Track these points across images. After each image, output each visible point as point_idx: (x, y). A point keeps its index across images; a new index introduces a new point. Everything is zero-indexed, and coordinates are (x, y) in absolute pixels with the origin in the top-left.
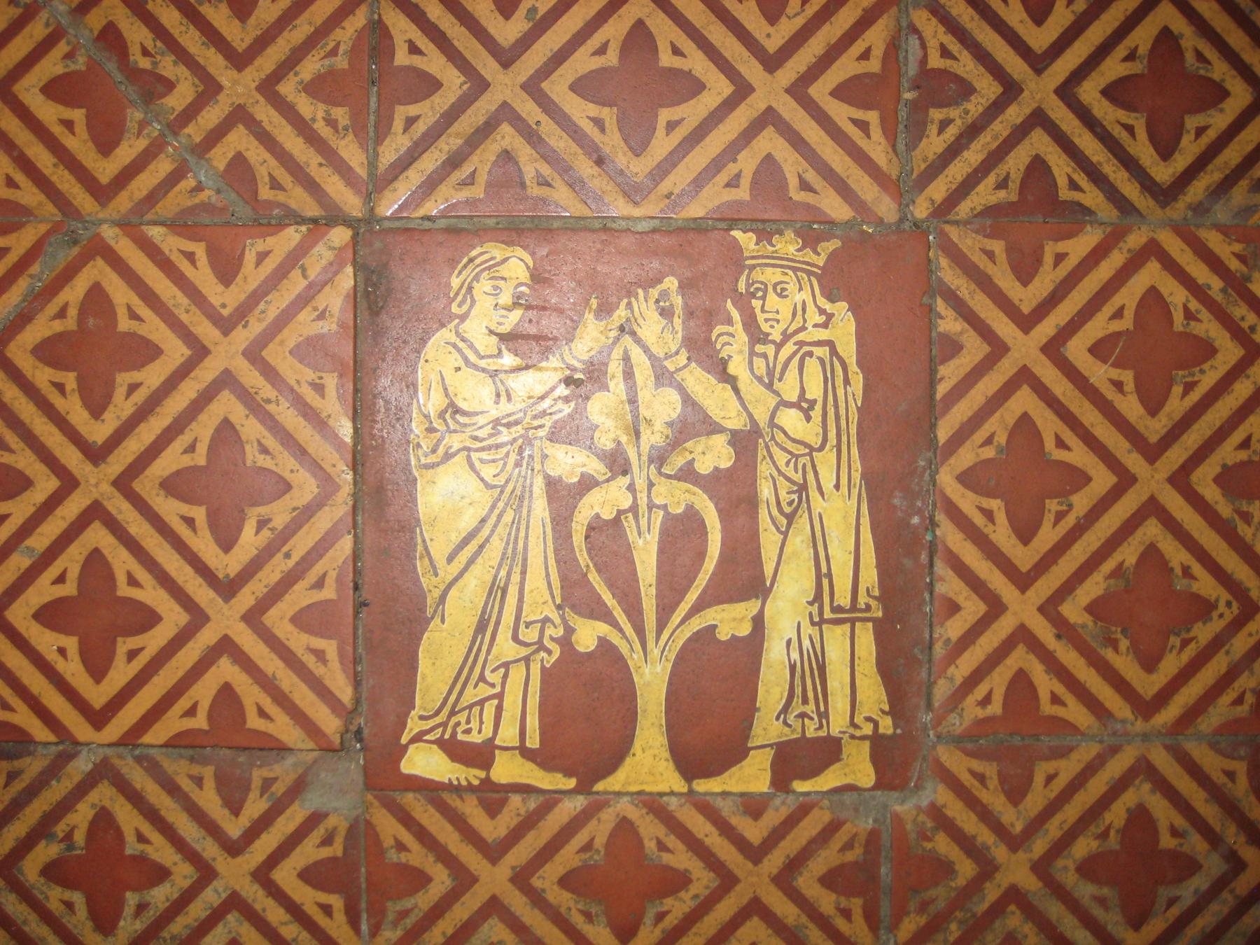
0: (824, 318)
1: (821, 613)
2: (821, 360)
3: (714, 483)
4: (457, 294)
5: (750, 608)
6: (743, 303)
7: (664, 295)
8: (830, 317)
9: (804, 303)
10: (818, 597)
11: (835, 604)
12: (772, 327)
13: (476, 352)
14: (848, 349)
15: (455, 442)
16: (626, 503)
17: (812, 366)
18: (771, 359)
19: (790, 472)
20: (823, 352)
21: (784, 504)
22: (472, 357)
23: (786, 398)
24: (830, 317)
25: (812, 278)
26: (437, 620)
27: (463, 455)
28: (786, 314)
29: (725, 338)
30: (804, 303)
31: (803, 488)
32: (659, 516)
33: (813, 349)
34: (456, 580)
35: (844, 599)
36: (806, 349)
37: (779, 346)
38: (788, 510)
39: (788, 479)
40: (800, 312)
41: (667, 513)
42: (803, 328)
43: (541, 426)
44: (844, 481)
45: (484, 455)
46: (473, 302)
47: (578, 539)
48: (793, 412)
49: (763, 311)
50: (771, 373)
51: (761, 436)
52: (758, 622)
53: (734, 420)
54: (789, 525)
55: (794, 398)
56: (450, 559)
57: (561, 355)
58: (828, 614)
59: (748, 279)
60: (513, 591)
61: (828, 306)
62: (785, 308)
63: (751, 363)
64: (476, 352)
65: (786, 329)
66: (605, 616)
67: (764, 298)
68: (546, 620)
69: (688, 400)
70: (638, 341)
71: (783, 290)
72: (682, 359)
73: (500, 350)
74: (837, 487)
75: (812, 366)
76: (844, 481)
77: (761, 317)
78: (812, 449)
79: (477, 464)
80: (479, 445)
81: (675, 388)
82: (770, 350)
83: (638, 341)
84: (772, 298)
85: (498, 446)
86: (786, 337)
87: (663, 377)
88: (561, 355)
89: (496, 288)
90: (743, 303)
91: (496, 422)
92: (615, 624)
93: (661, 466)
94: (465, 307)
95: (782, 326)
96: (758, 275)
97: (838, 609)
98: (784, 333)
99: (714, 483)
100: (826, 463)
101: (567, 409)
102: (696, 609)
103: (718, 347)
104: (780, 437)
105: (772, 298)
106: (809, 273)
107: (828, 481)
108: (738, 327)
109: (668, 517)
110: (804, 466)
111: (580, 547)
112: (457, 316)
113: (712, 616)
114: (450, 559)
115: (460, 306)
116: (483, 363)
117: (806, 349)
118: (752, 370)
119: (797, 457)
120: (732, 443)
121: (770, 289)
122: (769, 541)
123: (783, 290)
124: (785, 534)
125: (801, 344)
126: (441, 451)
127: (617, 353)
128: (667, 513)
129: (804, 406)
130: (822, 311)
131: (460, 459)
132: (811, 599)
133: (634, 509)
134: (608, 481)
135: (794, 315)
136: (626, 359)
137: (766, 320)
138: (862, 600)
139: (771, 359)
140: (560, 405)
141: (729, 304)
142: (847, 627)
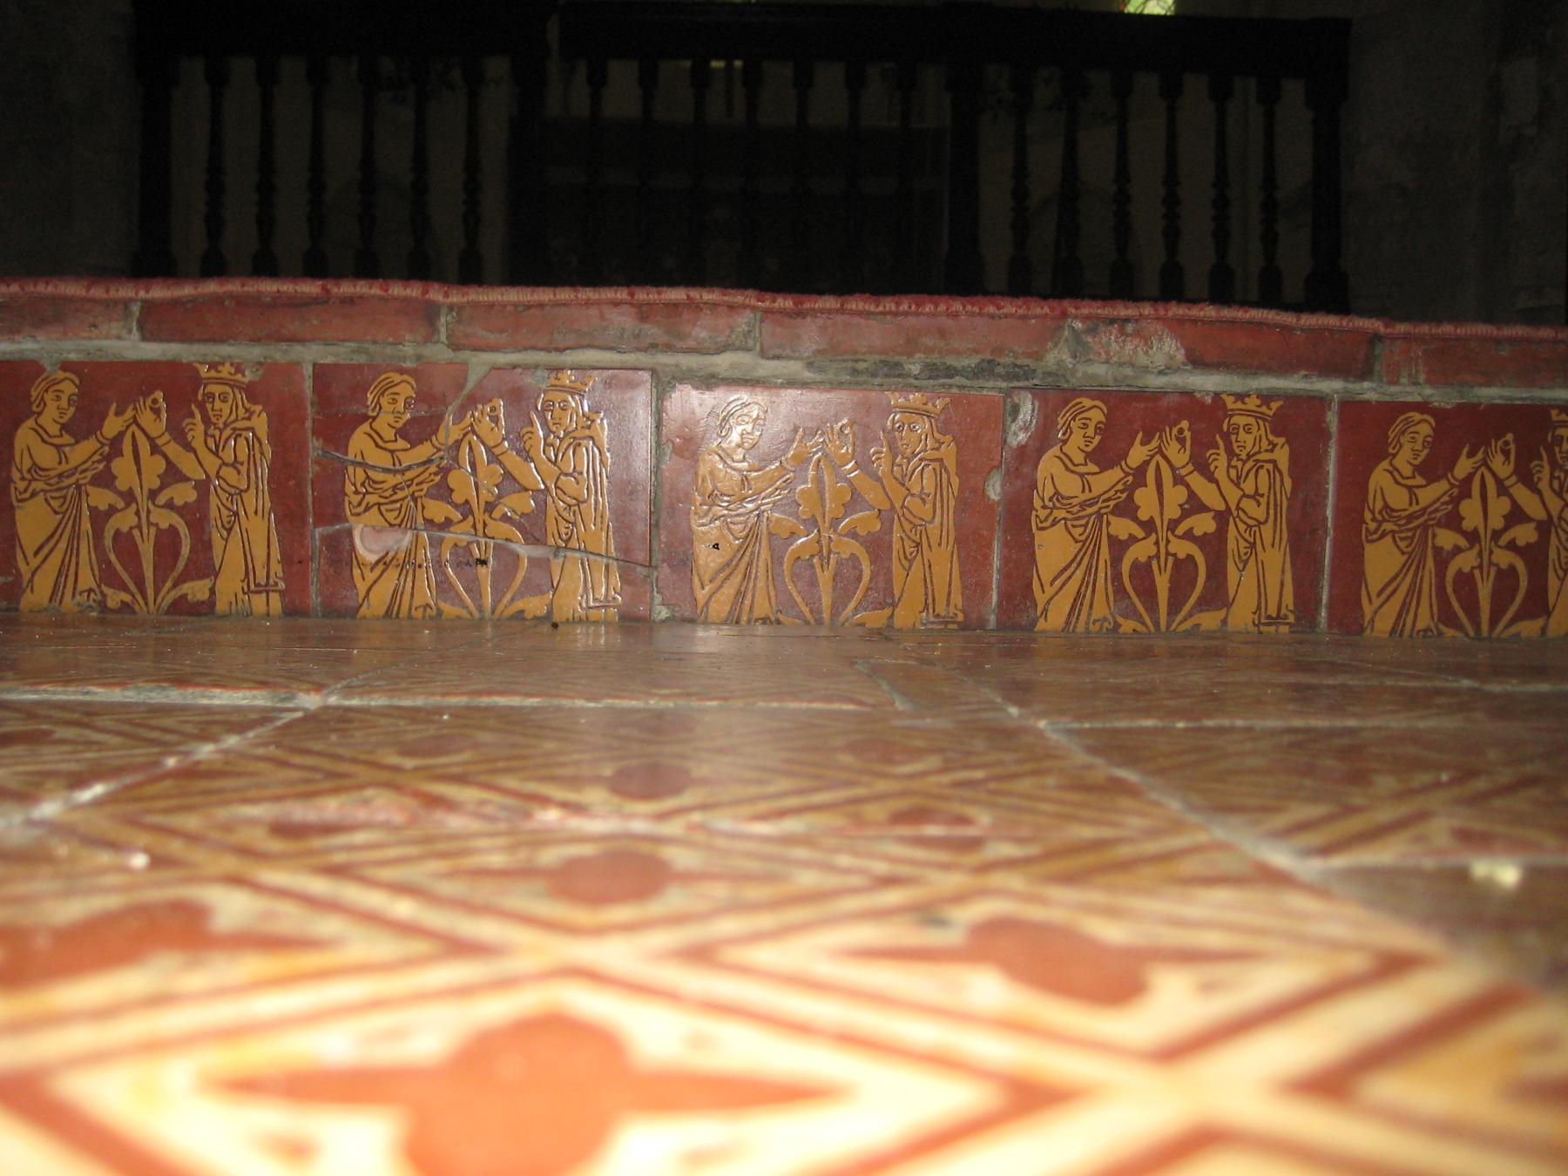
0: (1271, 446)
1: (1259, 618)
2: (1268, 471)
3: (1201, 541)
4: (35, 401)
5: (207, 583)
6: (1226, 437)
7: (1506, 443)
8: (1275, 445)
9: (1260, 436)
10: (1259, 608)
11: (257, 581)
12: (1241, 451)
13: (1401, 475)
14: (1284, 465)
15: (372, 499)
16: (1153, 551)
17: (242, 442)
18: (217, 439)
19: (1247, 536)
20: (1270, 466)
21: (1242, 554)
22: (1070, 465)
23: (1247, 492)
24: (1275, 445)
25: (1266, 424)
26: (28, 591)
27: (376, 508)
28: (226, 411)
29: (190, 427)
30: (1260, 436)
31: (1253, 545)
32: (153, 530)
33: (1265, 464)
34: (38, 567)
35: (1272, 612)
36: (238, 432)
37: (1244, 462)
38: (227, 526)
39: (1246, 540)
40: (1258, 441)
41: (158, 529)
42: (1259, 452)
43: (422, 490)
44: (1277, 541)
45: (389, 507)
46: (45, 405)
47: (108, 542)
48: (231, 469)
49: (213, 410)
50: (1239, 477)
51: (1232, 514)
52: (212, 591)
53: (1540, 514)
54: (229, 534)
55: (1252, 493)
56: (36, 553)
57: (96, 437)
58: (252, 587)
59: (1229, 422)
60: (749, 596)
61: (248, 405)
62: (1249, 439)
63: (1228, 471)
64: (1401, 475)
65: (226, 421)
66: (126, 589)
67: (1237, 434)
68: (90, 591)
69: (1514, 503)
70: (1490, 469)
71: (225, 397)
72: (1514, 479)
73: (61, 434)
74: (256, 513)
75: (1263, 473)
76: (1277, 541)
77: (1235, 445)
78: (1260, 523)
79: (384, 513)
80: (386, 501)
81: (1184, 485)
82: (217, 433)
83: (1490, 469)
84: (218, 404)
85: (1083, 517)
86: (226, 425)
87: (1179, 480)
88: (96, 437)
89: (58, 396)
90: (202, 407)
91: (60, 476)
92: (1144, 623)
93: (491, 514)
94: (1396, 450)
95: (224, 418)
96: (1235, 419)
97: (1269, 617)
98: (1248, 455)
99: (1201, 541)
100: (1267, 531)
101: (101, 466)
102: (1190, 615)
103: (186, 430)
104: (1242, 515)
105: (218, 404)
106: (1264, 420)
107: (1268, 539)
108: (1222, 451)
109: (1500, 571)
110: (1255, 532)
111: (109, 546)
112: (35, 413)
113: (187, 588)
114: (36, 553)
115: (38, 406)
116: (1403, 482)
117: (238, 432)
118: (1229, 477)
119: (570, 506)
120: (195, 487)
121: (1241, 429)
122: (218, 544)
123: (1249, 429)
124: (227, 541)
125: (1257, 461)
126: (30, 490)
127: (1479, 473)
128: (158, 529)
129: (1256, 497)
130: (1270, 443)
131: (1389, 538)
132: (1254, 611)
133: (1480, 567)
134: (1144, 538)
135: (231, 412)
136: (1483, 476)
137: (1238, 447)
138: (1283, 611)
139: (217, 439)
140: (1119, 494)
141: (193, 406)
142: (264, 595)
